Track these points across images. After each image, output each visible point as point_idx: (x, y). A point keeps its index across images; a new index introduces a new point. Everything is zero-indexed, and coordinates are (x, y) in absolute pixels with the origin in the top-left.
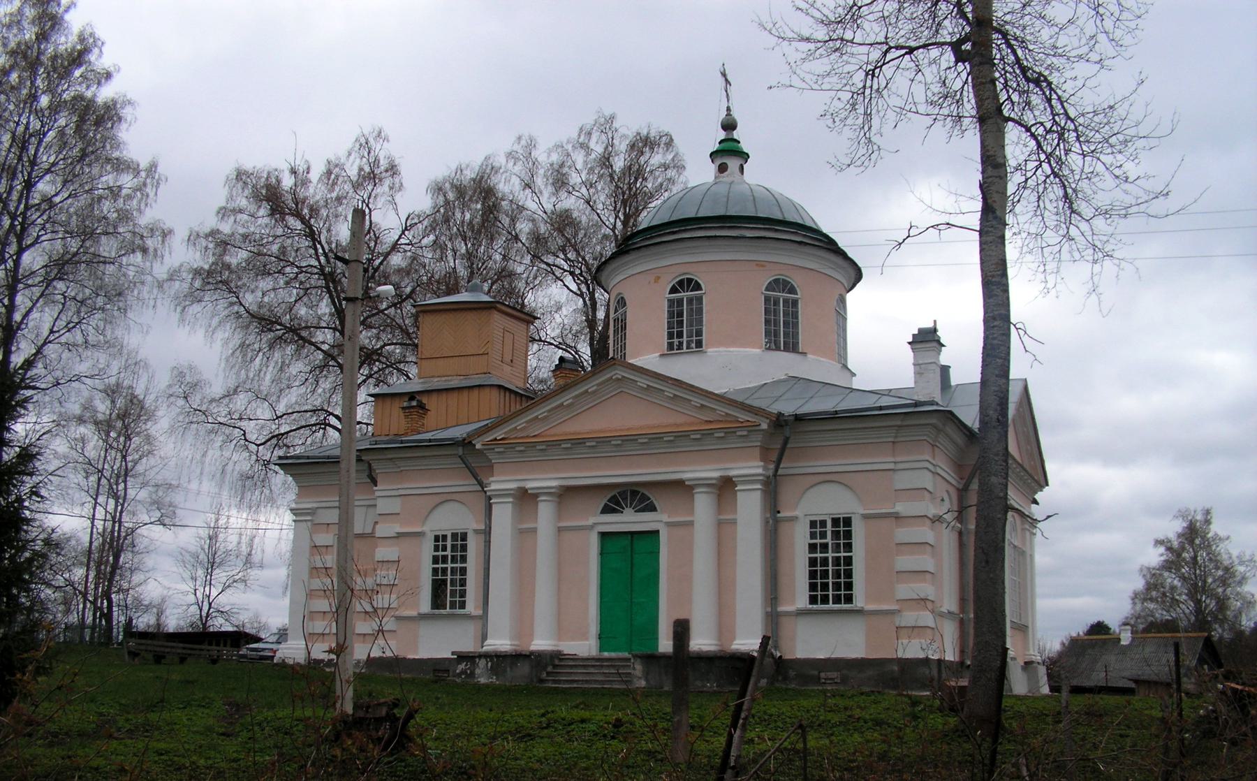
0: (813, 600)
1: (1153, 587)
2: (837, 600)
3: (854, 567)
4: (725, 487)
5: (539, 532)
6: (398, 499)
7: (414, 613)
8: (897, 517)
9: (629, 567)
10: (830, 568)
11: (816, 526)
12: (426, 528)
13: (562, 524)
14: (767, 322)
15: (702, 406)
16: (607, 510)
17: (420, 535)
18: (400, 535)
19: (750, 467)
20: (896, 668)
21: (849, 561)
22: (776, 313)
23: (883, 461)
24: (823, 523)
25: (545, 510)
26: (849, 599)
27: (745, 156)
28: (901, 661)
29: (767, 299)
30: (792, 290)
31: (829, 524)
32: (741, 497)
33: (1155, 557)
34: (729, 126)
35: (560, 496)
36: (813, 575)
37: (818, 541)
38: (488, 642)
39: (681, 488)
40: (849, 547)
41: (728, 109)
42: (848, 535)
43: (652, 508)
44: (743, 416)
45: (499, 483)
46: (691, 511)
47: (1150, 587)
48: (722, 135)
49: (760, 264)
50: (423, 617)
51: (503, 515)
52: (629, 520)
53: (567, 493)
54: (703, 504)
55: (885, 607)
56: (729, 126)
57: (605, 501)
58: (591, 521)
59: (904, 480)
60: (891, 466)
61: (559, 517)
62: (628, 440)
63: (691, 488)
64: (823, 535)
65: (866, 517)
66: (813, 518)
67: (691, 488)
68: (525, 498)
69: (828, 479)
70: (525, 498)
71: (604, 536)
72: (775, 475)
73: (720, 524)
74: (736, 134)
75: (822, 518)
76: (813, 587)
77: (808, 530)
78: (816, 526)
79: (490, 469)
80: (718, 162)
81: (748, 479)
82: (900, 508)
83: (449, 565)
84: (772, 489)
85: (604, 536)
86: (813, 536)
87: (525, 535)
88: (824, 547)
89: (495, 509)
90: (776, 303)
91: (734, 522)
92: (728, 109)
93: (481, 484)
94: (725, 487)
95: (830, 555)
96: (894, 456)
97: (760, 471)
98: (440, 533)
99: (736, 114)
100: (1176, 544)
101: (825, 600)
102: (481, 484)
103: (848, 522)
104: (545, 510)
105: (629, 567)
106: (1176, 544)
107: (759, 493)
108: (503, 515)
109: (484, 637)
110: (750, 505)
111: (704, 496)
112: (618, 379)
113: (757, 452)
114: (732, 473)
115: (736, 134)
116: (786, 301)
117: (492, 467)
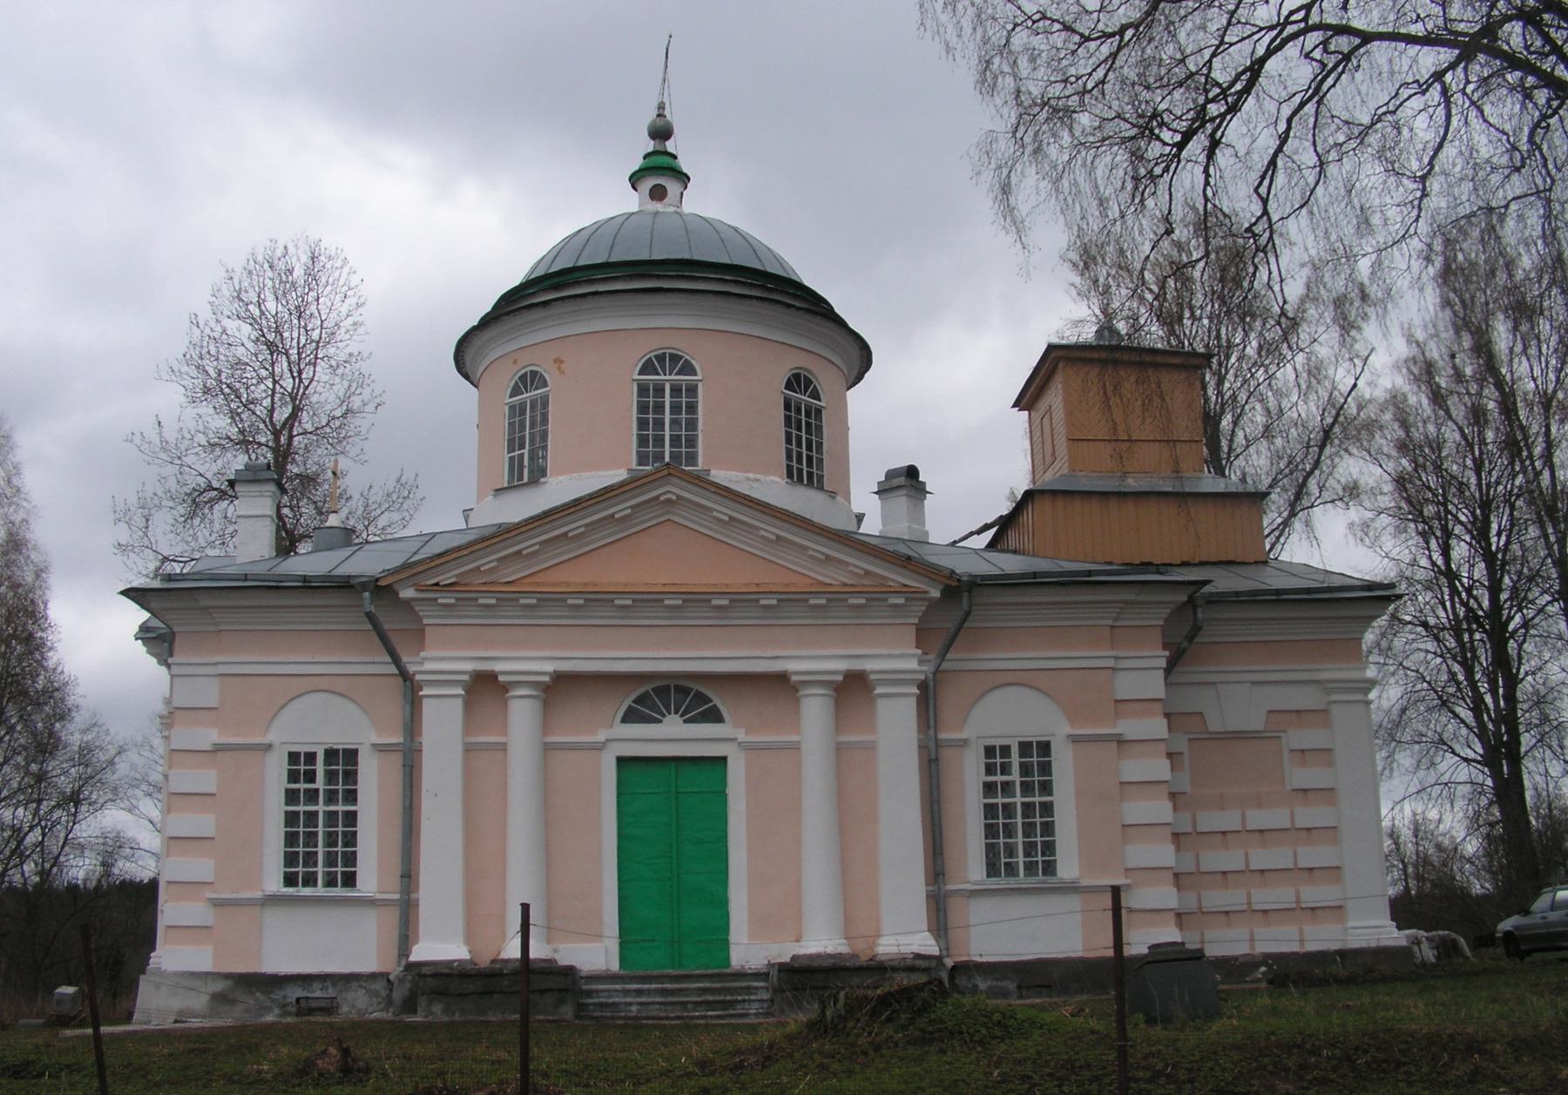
0: (290, 880)
2: (331, 882)
3: (283, 829)
4: (852, 689)
5: (804, 747)
6: (216, 680)
7: (258, 894)
8: (1121, 741)
9: (672, 820)
10: (1019, 820)
11: (995, 755)
12: (271, 737)
13: (843, 739)
15: (828, 558)
16: (630, 717)
17: (268, 747)
18: (219, 749)
19: (894, 657)
21: (351, 818)
23: (1101, 656)
24: (311, 758)
25: (522, 713)
26: (350, 880)
27: (683, 178)
29: (643, 390)
30: (688, 369)
31: (1015, 751)
32: (883, 707)
34: (661, 132)
35: (836, 690)
36: (291, 839)
37: (999, 778)
38: (415, 949)
39: (780, 684)
40: (351, 796)
41: (661, 107)
42: (1046, 768)
43: (714, 716)
44: (898, 577)
45: (444, 659)
46: (504, 730)
48: (650, 146)
50: (272, 900)
51: (443, 720)
52: (671, 735)
53: (560, 689)
54: (815, 710)
56: (661, 132)
57: (628, 702)
58: (601, 736)
60: (1110, 663)
61: (546, 728)
62: (695, 600)
63: (505, 688)
64: (1005, 769)
65: (1076, 740)
66: (295, 749)
67: (505, 688)
68: (485, 688)
70: (485, 688)
71: (621, 761)
72: (937, 671)
73: (840, 749)
74: (670, 146)
75: (311, 749)
76: (290, 859)
77: (983, 760)
78: (995, 755)
79: (419, 635)
80: (648, 184)
81: (896, 678)
83: (321, 808)
84: (928, 696)
85: (621, 761)
86: (990, 769)
87: (481, 759)
88: (1007, 788)
89: (428, 707)
90: (659, 390)
91: (871, 747)
92: (661, 107)
93: (396, 660)
94: (852, 689)
95: (321, 808)
96: (1112, 648)
97: (913, 664)
98: (997, 742)
99: (674, 117)
101: (310, 880)
102: (396, 660)
103: (1045, 748)
104: (522, 713)
105: (672, 820)
107: (460, 702)
108: (443, 720)
109: (406, 939)
110: (895, 723)
111: (819, 699)
112: (669, 501)
113: (912, 632)
114: (868, 666)
115: (670, 146)
116: (676, 390)
117: (422, 631)
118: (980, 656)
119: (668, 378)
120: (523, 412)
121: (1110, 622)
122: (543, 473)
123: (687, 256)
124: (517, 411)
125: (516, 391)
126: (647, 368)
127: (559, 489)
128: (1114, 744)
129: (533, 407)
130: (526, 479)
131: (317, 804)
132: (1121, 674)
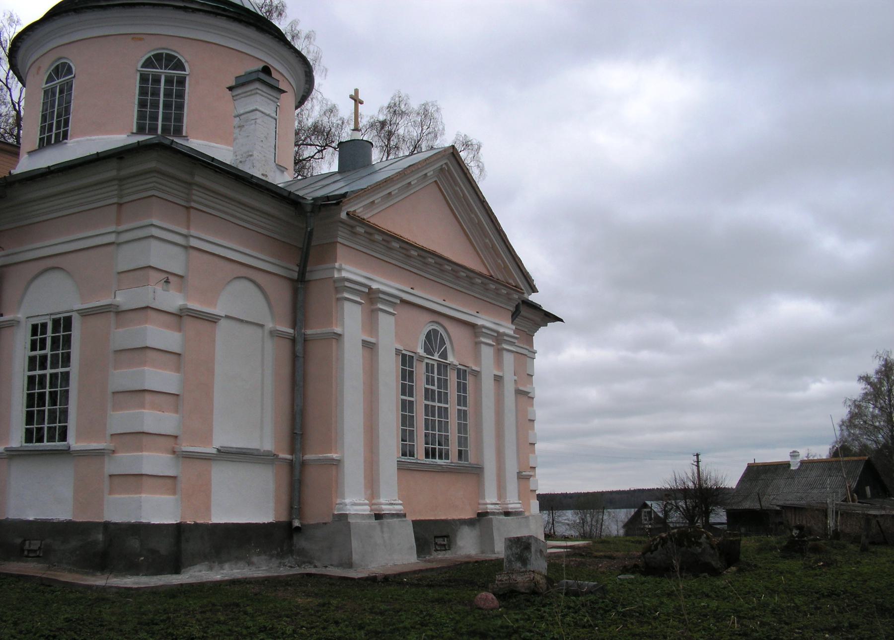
0: (29, 438)
1: (856, 417)
14: (142, 104)
20: (100, 537)
22: (156, 93)
23: (103, 231)
26: (63, 437)
28: (106, 525)
29: (144, 79)
30: (180, 66)
33: (858, 389)
47: (853, 416)
49: (136, 37)
50: (13, 454)
55: (94, 446)
59: (127, 258)
60: (112, 238)
65: (86, 313)
69: (51, 265)
77: (29, 338)
82: (122, 299)
90: (157, 80)
100: (874, 379)
106: (874, 379)
116: (169, 81)
118: (18, 250)
119: (163, 73)
120: (54, 94)
121: (115, 200)
122: (65, 136)
123: (304, 53)
124: (49, 93)
125: (50, 79)
126: (148, 63)
127: (77, 147)
128: (112, 315)
129: (61, 92)
130: (53, 142)
131: (51, 375)
132: (126, 248)
